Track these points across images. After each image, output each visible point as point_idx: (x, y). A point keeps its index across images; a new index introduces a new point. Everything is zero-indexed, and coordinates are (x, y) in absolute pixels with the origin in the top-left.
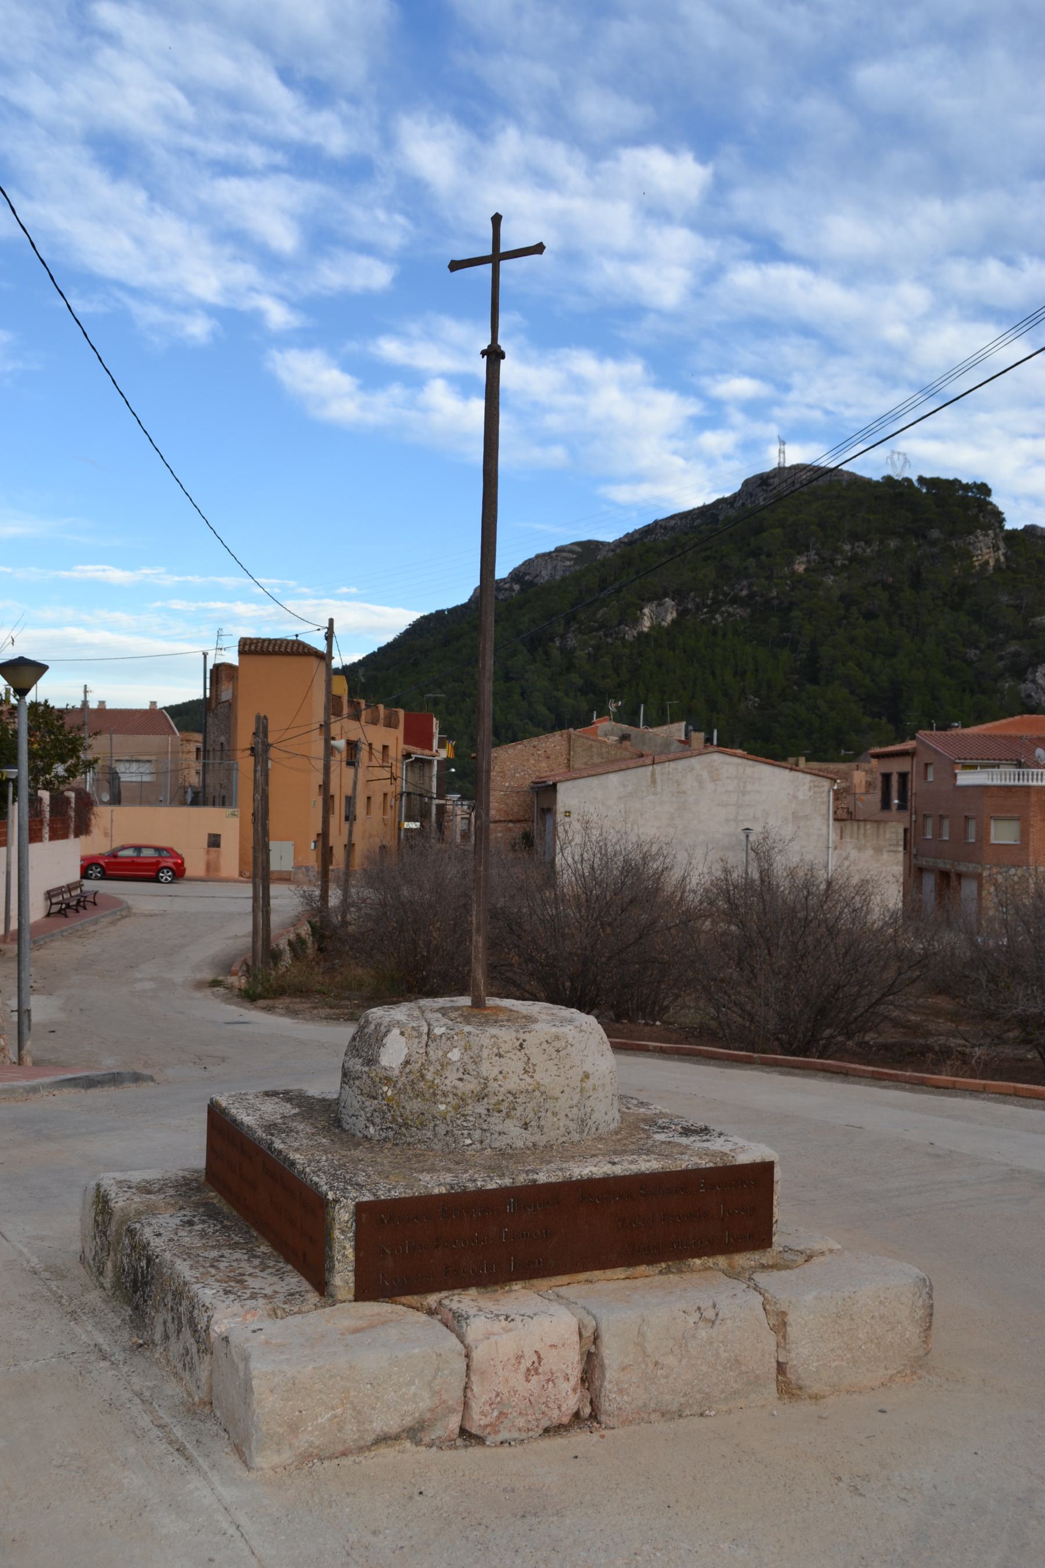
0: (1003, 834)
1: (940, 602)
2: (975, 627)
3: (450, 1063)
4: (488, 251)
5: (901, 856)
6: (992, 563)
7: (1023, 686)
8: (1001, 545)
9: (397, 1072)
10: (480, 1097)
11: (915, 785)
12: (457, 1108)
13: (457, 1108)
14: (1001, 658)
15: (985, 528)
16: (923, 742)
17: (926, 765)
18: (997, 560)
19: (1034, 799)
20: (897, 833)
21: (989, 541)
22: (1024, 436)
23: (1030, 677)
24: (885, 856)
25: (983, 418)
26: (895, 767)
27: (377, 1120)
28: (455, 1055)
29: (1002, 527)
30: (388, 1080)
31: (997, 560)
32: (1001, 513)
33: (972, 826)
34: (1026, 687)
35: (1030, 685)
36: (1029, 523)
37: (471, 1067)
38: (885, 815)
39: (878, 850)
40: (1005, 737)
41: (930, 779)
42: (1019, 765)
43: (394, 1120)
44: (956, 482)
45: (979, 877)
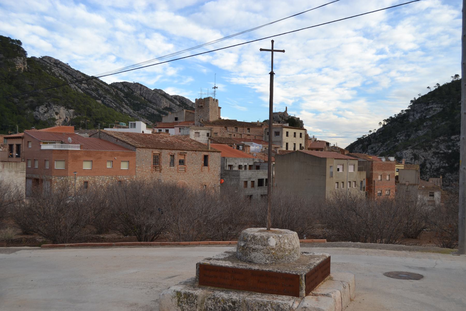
0: (59, 166)
1: (4, 81)
2: (17, 91)
3: (286, 243)
4: (271, 52)
5: (25, 174)
6: (23, 69)
7: (34, 113)
8: (26, 63)
9: (275, 247)
10: (293, 250)
11: (23, 149)
12: (289, 253)
13: (289, 253)
14: (26, 102)
15: (20, 56)
16: (27, 134)
17: (28, 142)
18: (25, 68)
19: (69, 154)
20: (23, 166)
21: (22, 61)
22: (28, 23)
23: (37, 110)
24: (19, 174)
25: (13, 14)
26: (15, 142)
27: (270, 259)
28: (286, 241)
29: (26, 57)
30: (273, 249)
31: (25, 68)
32: (25, 52)
33: (47, 164)
34: (35, 113)
35: (37, 112)
36: (33, 56)
37: (290, 243)
38: (10, 159)
39: (17, 172)
40: (55, 133)
41: (30, 146)
42: (62, 143)
43: (275, 258)
44: (8, 39)
45: (51, 180)
